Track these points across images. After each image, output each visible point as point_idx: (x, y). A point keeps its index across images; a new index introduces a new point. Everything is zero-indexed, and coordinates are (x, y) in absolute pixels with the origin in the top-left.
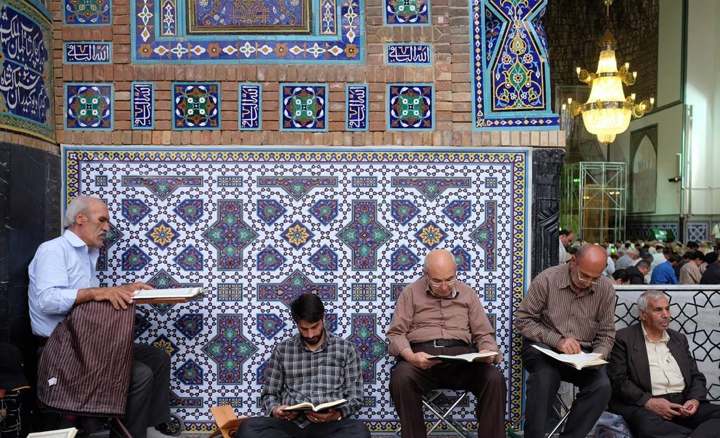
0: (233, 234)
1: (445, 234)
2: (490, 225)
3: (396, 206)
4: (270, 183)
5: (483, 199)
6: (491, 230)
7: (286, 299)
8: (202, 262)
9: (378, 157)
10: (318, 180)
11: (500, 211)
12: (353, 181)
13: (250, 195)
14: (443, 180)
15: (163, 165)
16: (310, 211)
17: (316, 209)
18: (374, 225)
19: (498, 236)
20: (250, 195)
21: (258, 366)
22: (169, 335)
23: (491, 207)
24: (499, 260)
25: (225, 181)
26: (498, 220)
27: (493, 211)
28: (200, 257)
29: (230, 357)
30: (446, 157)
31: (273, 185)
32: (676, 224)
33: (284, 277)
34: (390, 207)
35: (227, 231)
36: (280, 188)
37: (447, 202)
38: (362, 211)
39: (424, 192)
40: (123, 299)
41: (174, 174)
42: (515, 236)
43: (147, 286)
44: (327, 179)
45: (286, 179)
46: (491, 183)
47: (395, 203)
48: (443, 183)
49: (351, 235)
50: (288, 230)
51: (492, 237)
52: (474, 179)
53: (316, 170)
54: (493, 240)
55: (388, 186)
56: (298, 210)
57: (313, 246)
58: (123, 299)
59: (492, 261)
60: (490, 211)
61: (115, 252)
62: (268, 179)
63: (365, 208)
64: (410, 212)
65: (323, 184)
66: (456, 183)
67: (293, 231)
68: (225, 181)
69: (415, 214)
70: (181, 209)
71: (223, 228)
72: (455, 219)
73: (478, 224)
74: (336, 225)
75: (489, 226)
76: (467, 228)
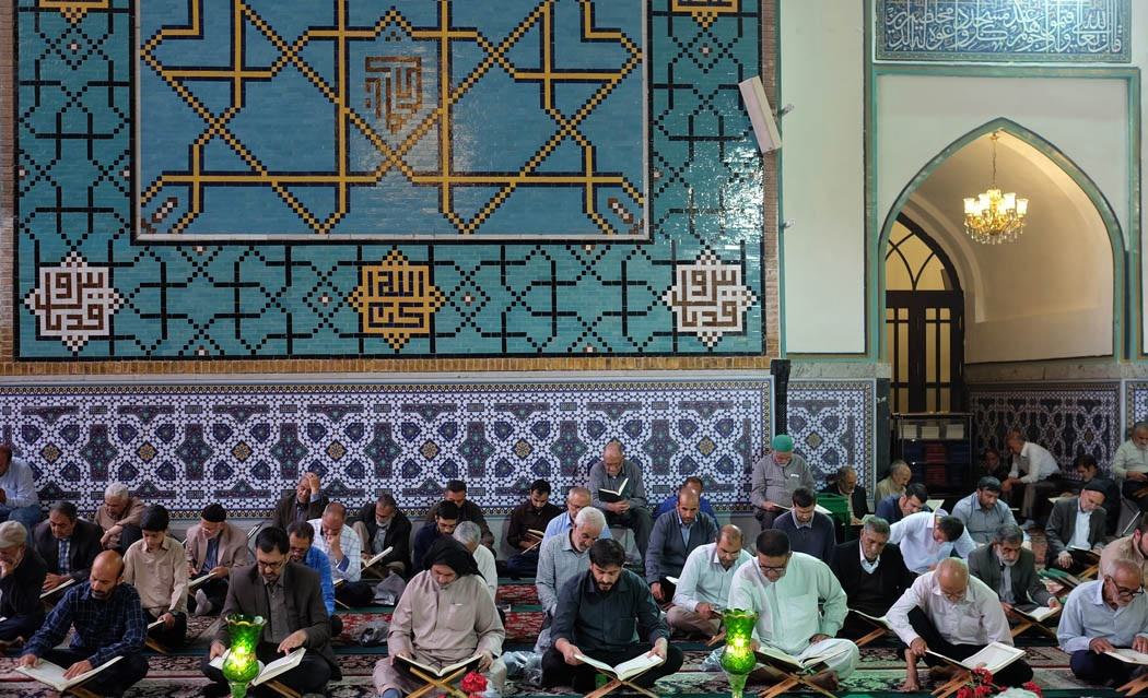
5: (306, 414)
17: (595, 436)
23: (851, 420)
24: (856, 457)
25: (379, 408)
29: (289, 458)
32: (754, 397)
44: (449, 406)
46: (851, 403)
51: (852, 440)
52: (459, 404)
63: (194, 430)
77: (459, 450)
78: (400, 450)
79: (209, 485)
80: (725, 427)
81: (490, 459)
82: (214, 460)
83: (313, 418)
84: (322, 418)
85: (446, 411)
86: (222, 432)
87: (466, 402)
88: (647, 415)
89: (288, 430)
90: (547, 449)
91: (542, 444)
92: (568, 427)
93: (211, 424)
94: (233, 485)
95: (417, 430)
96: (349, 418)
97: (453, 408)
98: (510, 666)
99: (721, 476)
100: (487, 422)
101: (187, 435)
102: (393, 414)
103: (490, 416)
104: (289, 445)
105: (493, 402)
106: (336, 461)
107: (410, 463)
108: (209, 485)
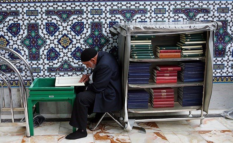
0: (95, 41)
1: (72, 41)
2: (58, 13)
4: (178, 11)
5: (109, 15)
6: (188, 11)
12: (36, 11)
13: (42, 20)
14: (70, 11)
18: (38, 37)
20: (42, 20)
25: (30, 13)
28: (48, 53)
36: (120, 15)
38: (221, 52)
39: (61, 18)
41: (197, 6)
44: (78, 11)
45: (123, 10)
48: (70, 13)
49: (27, 42)
51: (64, 12)
52: (85, 9)
54: (67, 11)
55: (108, 14)
56: (65, 28)
57: (70, 34)
62: (115, 10)
64: (14, 32)
65: (203, 12)
66: (12, 14)
68: (30, 13)
69: (57, 30)
71: (93, 37)
72: (54, 51)
77: (22, 42)
78: (45, 42)
79: (44, 63)
80: (78, 28)
81: (43, 48)
82: (47, 47)
83: (49, 19)
84: (55, 19)
85: (12, 15)
86: (52, 29)
87: (25, 9)
88: (87, 19)
89: (33, 27)
90: (48, 42)
91: (15, 39)
92: (33, 27)
93: (44, 23)
94: (59, 64)
95: (15, 34)
96: (74, 19)
97: (81, 12)
98: (229, 114)
99: (76, 21)
100: (40, 23)
101: (92, 29)
102: (39, 17)
103: (42, 19)
104: (33, 38)
105: (44, 9)
106: (65, 48)
107: (52, 50)
108: (44, 63)
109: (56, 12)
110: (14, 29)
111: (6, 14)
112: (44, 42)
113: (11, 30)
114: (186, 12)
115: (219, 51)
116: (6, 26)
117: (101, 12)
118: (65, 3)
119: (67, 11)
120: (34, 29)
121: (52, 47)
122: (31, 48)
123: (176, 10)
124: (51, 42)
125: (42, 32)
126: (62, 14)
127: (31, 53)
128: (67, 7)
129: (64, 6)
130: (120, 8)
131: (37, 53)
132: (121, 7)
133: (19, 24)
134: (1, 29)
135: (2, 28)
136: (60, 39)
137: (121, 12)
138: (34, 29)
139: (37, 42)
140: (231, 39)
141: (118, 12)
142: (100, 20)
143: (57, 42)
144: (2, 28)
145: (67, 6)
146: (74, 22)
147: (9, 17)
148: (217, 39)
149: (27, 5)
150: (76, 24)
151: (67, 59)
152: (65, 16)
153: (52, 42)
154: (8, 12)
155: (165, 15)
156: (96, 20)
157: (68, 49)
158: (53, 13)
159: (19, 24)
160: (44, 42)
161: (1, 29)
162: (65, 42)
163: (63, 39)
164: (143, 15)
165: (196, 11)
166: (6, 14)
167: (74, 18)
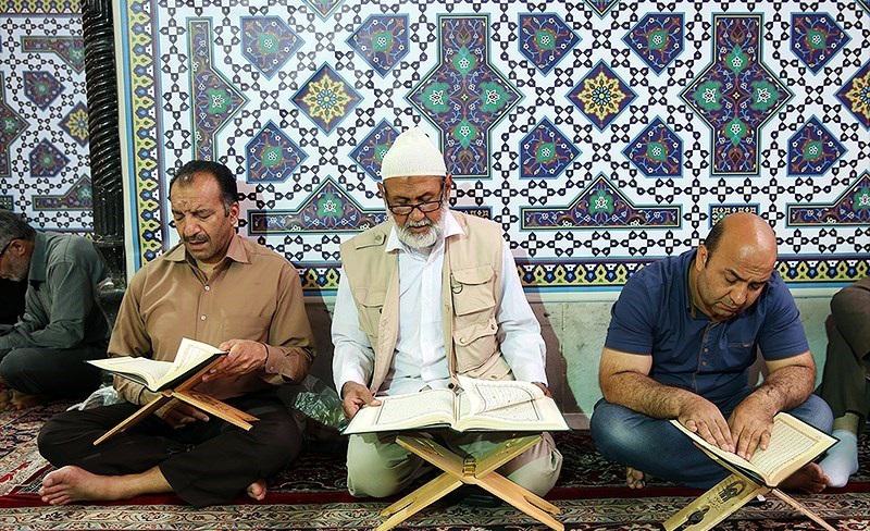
2: (624, 214)
3: (671, 165)
4: (657, 215)
7: (212, 123)
8: (807, 173)
9: (826, 269)
10: (196, 59)
11: (656, 234)
15: (601, 254)
16: (67, 161)
19: (601, 232)
21: (53, 73)
22: (60, 116)
24: (810, 232)
26: (189, 139)
27: (658, 221)
30: (832, 272)
31: (651, 210)
33: (17, 108)
34: (390, 12)
35: (472, 107)
37: (297, 178)
38: (459, 40)
39: (615, 196)
40: (437, 362)
42: (803, 264)
43: (731, 420)
44: (545, 224)
45: (624, 223)
47: (400, 23)
48: (578, 215)
50: (622, 108)
51: (602, 220)
53: (63, 220)
54: (854, 220)
57: (844, 126)
58: (437, 362)
59: (809, 219)
60: (38, 46)
61: (19, 150)
66: (203, 49)
67: (592, 106)
70: (263, 63)
73: (18, 143)
74: (777, 31)
75: (624, 214)
76: (27, 142)
84: (641, 191)
86: (656, 151)
90: (529, 97)
96: (562, 192)
97: (800, 215)
100: (514, 177)
109: (366, 222)
110: (814, 150)
111: (844, 212)
112: (510, 97)
113: (285, 152)
114: (353, 218)
115: (467, 46)
116: (305, 169)
117: (721, 210)
118: (858, 251)
119: (588, 224)
120: (730, 153)
121: (658, 71)
122: (750, 69)
123: (668, 220)
124: (660, 96)
125: (697, 136)
126: (611, 211)
127: (478, 51)
128: (649, 245)
129: (601, 244)
130: (638, 232)
131: (450, 51)
132: (632, 236)
133: (32, 175)
134: (866, 150)
135: (861, 156)
136: (67, 119)
137: (631, 216)
138: (731, 152)
139: (447, 97)
140: (779, 96)
141: (644, 214)
142: (722, 183)
143: (635, 96)
144: (861, 156)
145: (588, 244)
146: (829, 175)
147: (831, 201)
148: (720, 96)
149: (802, 246)
150: (52, 173)
151: (595, 19)
152: (601, 203)
153: (545, 96)
154: (833, 222)
155: (714, 200)
156: (735, 181)
157: (588, 64)
158: (648, 216)
159: (32, 175)
160: (510, 97)
161: (866, 150)
162: (327, 99)
163: (337, 109)
164: (804, 201)
165: (847, 212)
166: (844, 212)
167: (827, 192)
